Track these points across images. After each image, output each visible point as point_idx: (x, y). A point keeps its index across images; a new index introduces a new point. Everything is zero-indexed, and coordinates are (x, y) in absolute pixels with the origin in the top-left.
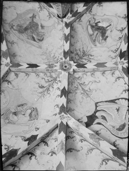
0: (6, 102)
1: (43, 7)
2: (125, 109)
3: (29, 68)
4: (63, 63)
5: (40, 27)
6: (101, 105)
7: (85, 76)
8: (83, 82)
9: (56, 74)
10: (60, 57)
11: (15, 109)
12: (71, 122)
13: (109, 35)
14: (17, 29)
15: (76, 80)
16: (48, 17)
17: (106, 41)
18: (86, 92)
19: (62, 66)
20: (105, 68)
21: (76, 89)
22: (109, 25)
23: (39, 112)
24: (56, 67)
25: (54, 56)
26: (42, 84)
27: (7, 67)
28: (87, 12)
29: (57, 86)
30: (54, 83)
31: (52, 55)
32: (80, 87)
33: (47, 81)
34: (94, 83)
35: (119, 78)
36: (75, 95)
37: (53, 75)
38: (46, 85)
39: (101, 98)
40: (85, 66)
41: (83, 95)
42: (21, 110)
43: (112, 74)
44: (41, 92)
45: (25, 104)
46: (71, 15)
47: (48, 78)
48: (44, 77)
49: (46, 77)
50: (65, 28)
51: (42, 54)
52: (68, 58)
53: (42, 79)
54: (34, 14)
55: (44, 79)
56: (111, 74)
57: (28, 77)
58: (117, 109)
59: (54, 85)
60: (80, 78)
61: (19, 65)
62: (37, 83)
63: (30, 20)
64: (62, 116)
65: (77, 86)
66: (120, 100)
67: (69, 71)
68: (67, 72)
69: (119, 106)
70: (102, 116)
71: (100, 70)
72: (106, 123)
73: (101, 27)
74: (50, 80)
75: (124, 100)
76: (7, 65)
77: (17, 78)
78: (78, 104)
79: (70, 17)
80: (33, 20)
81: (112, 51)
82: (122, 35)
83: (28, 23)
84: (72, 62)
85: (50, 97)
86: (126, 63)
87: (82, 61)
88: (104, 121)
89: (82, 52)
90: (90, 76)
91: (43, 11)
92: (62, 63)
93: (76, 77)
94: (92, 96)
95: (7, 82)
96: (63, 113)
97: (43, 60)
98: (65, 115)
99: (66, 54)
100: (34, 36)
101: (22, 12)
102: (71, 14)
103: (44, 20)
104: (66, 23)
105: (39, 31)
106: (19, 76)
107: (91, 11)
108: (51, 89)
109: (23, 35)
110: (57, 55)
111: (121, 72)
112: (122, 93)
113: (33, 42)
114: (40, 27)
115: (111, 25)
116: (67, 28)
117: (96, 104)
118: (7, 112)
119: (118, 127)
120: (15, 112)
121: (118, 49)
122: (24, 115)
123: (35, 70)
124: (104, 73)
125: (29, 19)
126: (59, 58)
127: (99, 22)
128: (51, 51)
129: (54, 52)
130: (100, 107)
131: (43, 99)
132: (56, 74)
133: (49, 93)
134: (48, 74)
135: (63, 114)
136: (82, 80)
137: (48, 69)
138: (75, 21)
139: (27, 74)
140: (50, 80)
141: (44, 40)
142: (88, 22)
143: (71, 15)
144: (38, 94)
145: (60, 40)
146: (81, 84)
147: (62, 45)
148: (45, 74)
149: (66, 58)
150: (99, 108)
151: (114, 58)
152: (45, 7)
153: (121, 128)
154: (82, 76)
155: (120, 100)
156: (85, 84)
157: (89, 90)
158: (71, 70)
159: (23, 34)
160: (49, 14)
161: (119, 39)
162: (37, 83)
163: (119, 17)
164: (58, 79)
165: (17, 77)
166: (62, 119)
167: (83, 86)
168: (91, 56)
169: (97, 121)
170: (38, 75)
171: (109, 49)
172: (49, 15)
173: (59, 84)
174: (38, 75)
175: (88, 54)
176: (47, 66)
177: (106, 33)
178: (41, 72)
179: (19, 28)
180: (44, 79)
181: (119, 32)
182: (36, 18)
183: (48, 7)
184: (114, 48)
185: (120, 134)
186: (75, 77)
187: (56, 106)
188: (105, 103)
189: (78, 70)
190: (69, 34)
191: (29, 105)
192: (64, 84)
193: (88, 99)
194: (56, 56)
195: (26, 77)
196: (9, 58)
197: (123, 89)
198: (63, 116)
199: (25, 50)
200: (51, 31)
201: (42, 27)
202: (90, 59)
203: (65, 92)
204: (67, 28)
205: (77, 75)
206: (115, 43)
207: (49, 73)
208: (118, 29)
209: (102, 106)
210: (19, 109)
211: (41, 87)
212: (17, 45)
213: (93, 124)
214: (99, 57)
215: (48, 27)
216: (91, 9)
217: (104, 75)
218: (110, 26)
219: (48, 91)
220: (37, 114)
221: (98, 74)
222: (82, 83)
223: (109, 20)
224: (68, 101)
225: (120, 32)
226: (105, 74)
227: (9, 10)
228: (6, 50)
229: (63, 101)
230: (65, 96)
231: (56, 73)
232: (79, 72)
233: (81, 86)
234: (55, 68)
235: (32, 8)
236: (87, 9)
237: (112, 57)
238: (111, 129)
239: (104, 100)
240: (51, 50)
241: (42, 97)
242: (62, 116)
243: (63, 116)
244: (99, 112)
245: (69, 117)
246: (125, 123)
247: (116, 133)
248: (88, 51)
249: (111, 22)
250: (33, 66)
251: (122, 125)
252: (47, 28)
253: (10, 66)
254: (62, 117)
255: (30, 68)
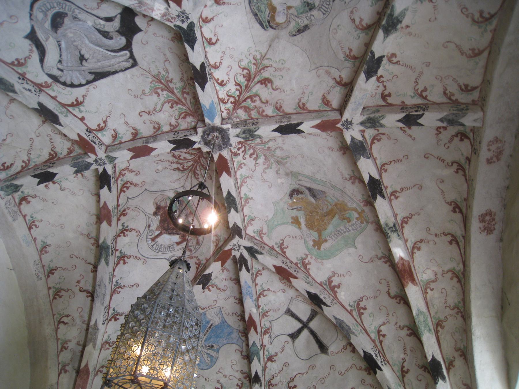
0: (335, 31)
1: (299, 265)
2: (67, 63)
3: (296, 122)
4: (224, 145)
5: (302, 220)
6: (124, 63)
7: (173, 122)
8: (174, 108)
9: (237, 117)
10: (240, 158)
11: (312, 17)
12: (159, 10)
13: (153, 217)
14: (350, 211)
15: (189, 109)
16: (285, 246)
17: (156, 204)
18: (163, 87)
19: (223, 138)
20: (130, 148)
21: (185, 88)
22: (157, 240)
23: (253, 19)
24: (237, 133)
25: (256, 159)
26: (266, 89)
27: (347, 120)
28: (204, 262)
29: (226, 88)
30: (239, 96)
31: (261, 160)
32: (179, 95)
33: (255, 99)
34: (152, 109)
35: (101, 129)
36: (182, 74)
37: (244, 113)
38: (257, 88)
39: (129, 76)
40: (173, 146)
41: (168, 79)
42: (298, 17)
43: (116, 135)
44: (266, 69)
45: (294, 33)
46: (233, 255)
47: (253, 104)
48: (263, 106)
49: (258, 106)
50: (240, 225)
51: (286, 161)
52: (216, 157)
53: (267, 102)
54: (319, 248)
55: (263, 102)
56: (120, 136)
57: (300, 100)
58: (86, 60)
59: (237, 90)
60: (183, 115)
61: (323, 127)
62: (278, 89)
63: (325, 234)
64: (184, 19)
65: (185, 95)
66: (84, 82)
67: (205, 128)
68: (210, 124)
69: (83, 68)
70: (111, 38)
71: (142, 140)
72: (95, 22)
73: (174, 234)
74: (249, 100)
75: (76, 83)
76: (348, 124)
77: (323, 95)
78: (169, 55)
79: (234, 249)
80: (320, 235)
81: (136, 185)
82: (120, 223)
83: (330, 229)
84: (205, 149)
85: (237, 60)
86: (92, 164)
87: (192, 154)
88: (102, 27)
89: (198, 175)
90: (162, 123)
91: (299, 257)
92: (226, 145)
93: (191, 117)
94: (150, 80)
95: (343, 83)
96: (186, 28)
97: (279, 147)
98: (179, 23)
99: (223, 166)
100: (312, 200)
101: (346, 250)
102: (234, 256)
103: (294, 237)
104: (241, 236)
105: (302, 212)
106: (320, 102)
107: (197, 266)
108: (242, 80)
109: (336, 199)
110: (250, 162)
111: (97, 143)
112: (84, 96)
113: (314, 186)
114: (302, 220)
115: (153, 240)
116: (235, 224)
117: (135, 64)
118: (327, 6)
119: (67, 21)
120: (310, 9)
121: (122, 190)
122: (289, 8)
123: (285, 120)
124: (135, 135)
125: (328, 238)
126: (242, 155)
127: (178, 244)
128: (266, 169)
129: (260, 169)
130: (122, 59)
131: (257, 54)
132: (237, 117)
133: (244, 69)
134: (254, 114)
135: (185, 26)
136: (177, 113)
137: (252, 127)
138: (227, 241)
139: (302, 107)
140: (249, 100)
141: (288, 193)
142: (200, 241)
143: (233, 253)
144: (271, 63)
145: (250, 197)
146: (178, 102)
147: (242, 185)
148: (261, 113)
149: (221, 156)
150: (126, 54)
151: (124, 170)
152: (294, 266)
153: (58, 19)
154: (180, 121)
155: (84, 82)
156: (170, 104)
157: (159, 91)
158: (200, 130)
159: (336, 201)
160: (284, 253)
161: (125, 212)
162: (278, 89)
163: (138, 258)
164: (229, 105)
165: (324, 98)
166: (183, 13)
167: (173, 97)
168: (178, 169)
169: (116, 24)
170: (278, 108)
171: (146, 189)
172: (285, 250)
173: (222, 95)
174: (278, 108)
175: (186, 172)
176: (256, 133)
177: (160, 223)
178: (270, 117)
179: (347, 215)
180: (263, 102)
181: (129, 227)
182: (314, 241)
183: (287, 268)
184: (132, 192)
185: (55, 5)
186: (193, 116)
187: (214, 40)
188: (116, 68)
189: (188, 133)
190: (229, 212)
191: (284, 33)
192: (207, 96)
193: (155, 73)
194: (252, 159)
195: (303, 101)
196: (348, 140)
197: (84, 106)
198: (183, 21)
199: (324, 165)
200: (275, 214)
201: (296, 221)
202: (177, 163)
203: (199, 76)
204: (235, 224)
205: (190, 122)
206: (131, 203)
207: (253, 116)
208: (133, 232)
209: (120, 60)
210: (305, 19)
211: (267, 82)
212: (342, 175)
213: (119, 16)
214: (160, 167)
215: (283, 224)
216: (197, 270)
217: (134, 131)
218: (153, 236)
219: (249, 74)
220: (256, 15)
221: (146, 131)
222: (177, 105)
223: (159, 249)
224: (185, 59)
225: (128, 226)
226: (132, 134)
227: (374, 253)
228: (359, 159)
229: (196, 57)
230: (194, 67)
231: (238, 120)
232: (187, 130)
233: (176, 96)
234: (238, 130)
235: (325, 261)
236: (205, 268)
237: (131, 171)
238: (79, 13)
239: (121, 74)
240: (266, 171)
241: (259, 57)
242: (184, 19)
243: (183, 21)
244: (122, 46)
245: (168, 20)
246: (56, 32)
247: (64, 5)
248: (189, 179)
249: (153, 246)
250: (289, 129)
251: (59, 25)
252: (285, 221)
253: (341, 123)
254: (183, 17)
255: (293, 123)
